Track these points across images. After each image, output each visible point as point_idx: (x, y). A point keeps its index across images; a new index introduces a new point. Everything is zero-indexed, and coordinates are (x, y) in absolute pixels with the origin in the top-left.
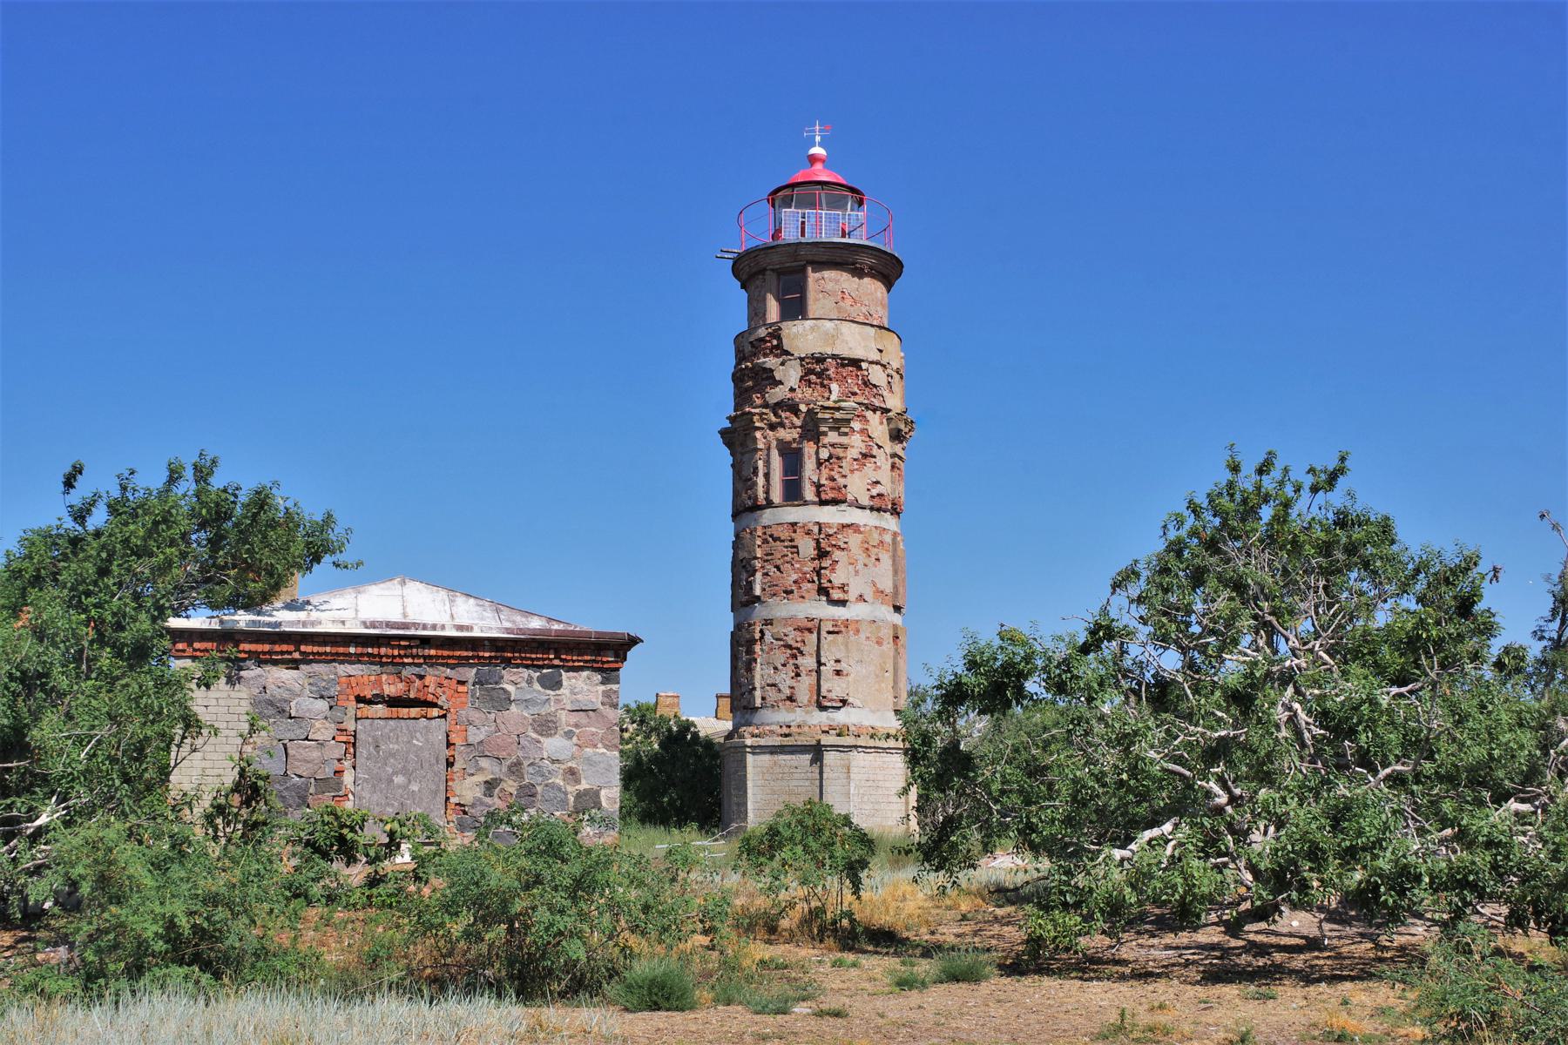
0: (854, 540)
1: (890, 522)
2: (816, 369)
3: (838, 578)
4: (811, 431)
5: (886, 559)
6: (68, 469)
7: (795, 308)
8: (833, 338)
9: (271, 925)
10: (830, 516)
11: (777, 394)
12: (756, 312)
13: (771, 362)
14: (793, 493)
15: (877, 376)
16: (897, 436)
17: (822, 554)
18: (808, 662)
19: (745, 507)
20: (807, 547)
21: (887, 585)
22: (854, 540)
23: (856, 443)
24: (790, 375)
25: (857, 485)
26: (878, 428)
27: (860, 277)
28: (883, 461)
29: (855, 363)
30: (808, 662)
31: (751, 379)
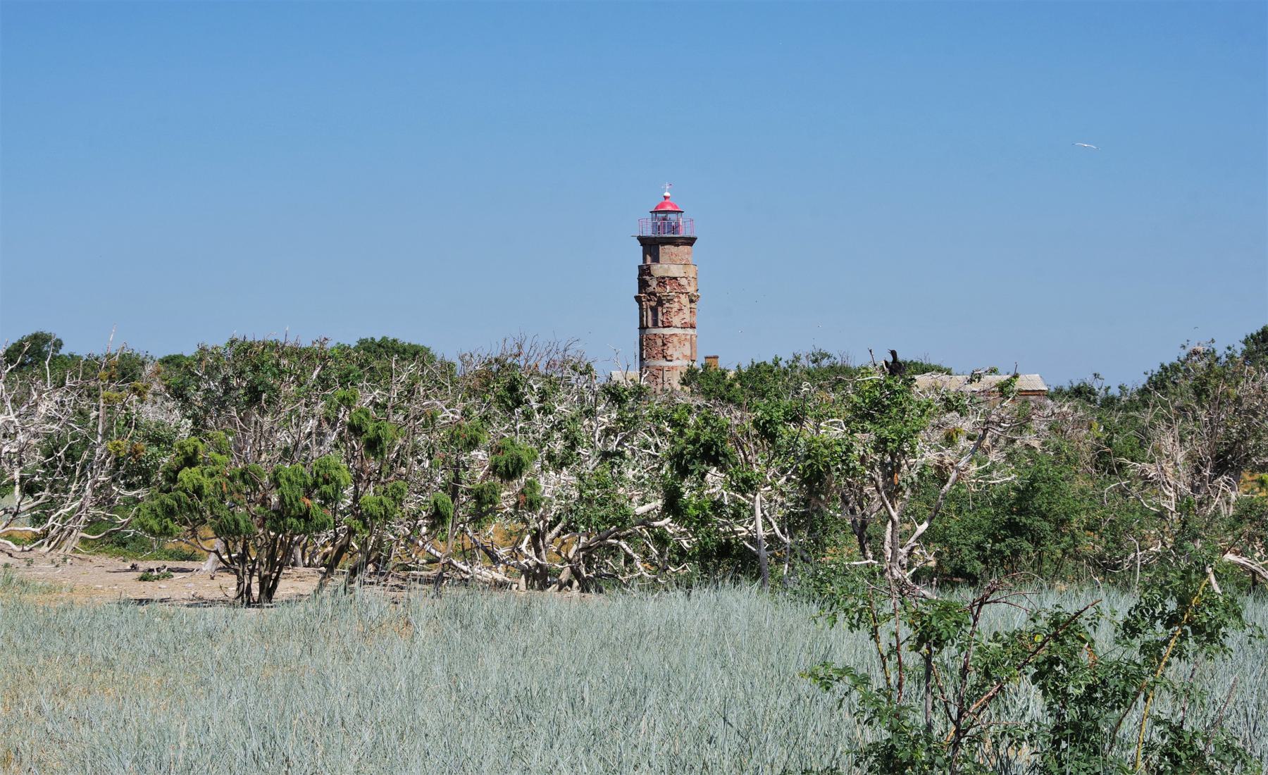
0: (675, 339)
1: (690, 331)
2: (662, 281)
3: (669, 352)
4: (660, 303)
5: (687, 344)
6: (944, 366)
7: (656, 259)
8: (667, 271)
9: (573, 680)
10: (667, 331)
11: (650, 289)
12: (645, 260)
13: (647, 278)
14: (655, 325)
15: (684, 282)
16: (691, 301)
17: (664, 345)
18: (660, 380)
19: (643, 328)
20: (659, 342)
21: (688, 353)
22: (675, 339)
23: (676, 306)
24: (654, 283)
25: (676, 321)
26: (684, 299)
27: (362, 342)
28: (686, 311)
29: (676, 278)
30: (660, 380)
31: (643, 284)
